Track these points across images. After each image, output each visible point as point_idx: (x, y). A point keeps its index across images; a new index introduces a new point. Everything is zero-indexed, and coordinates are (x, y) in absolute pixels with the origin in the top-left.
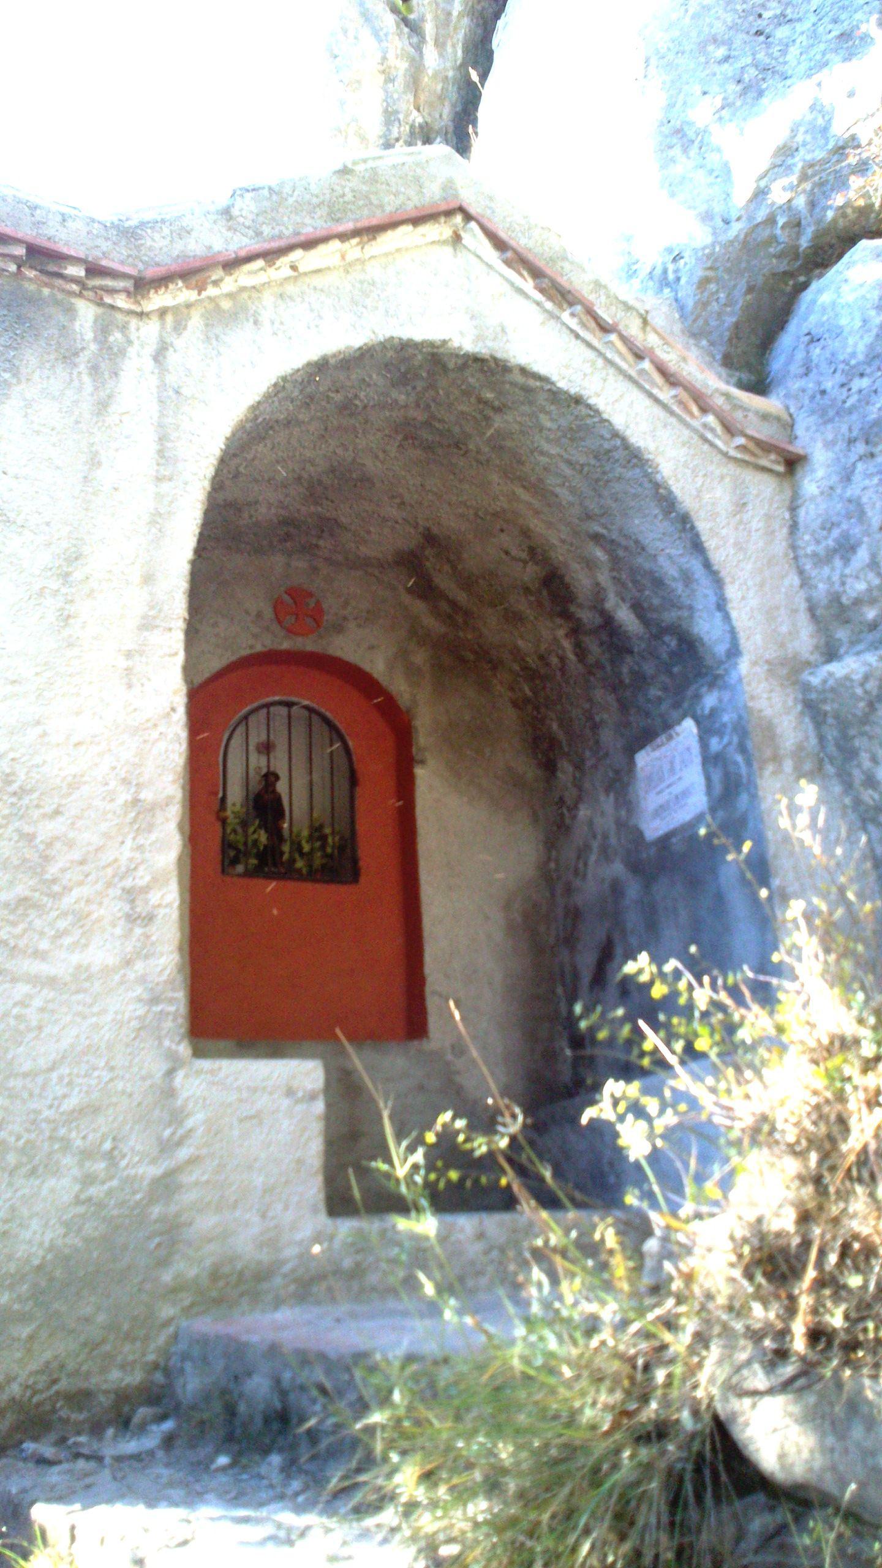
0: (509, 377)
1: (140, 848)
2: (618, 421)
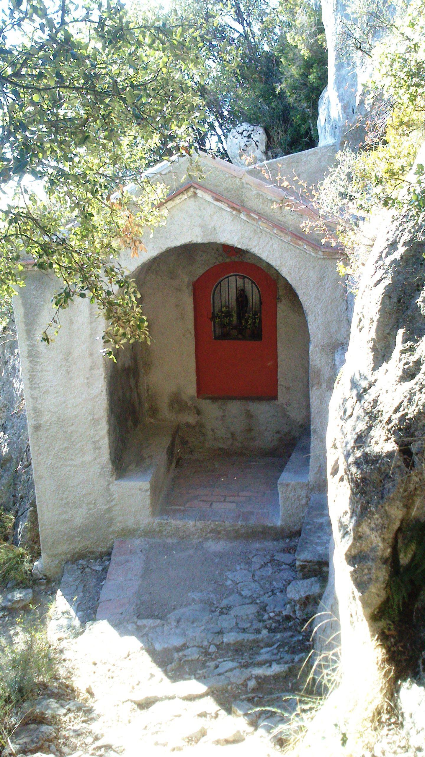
1: (96, 431)
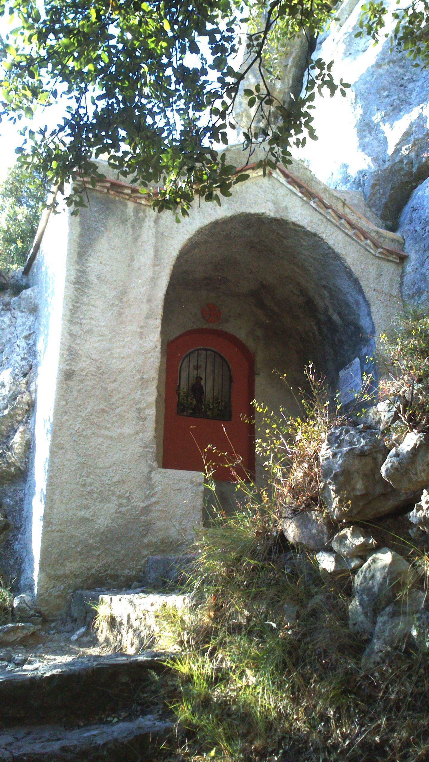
0: (288, 226)
1: (143, 395)
2: (331, 243)
